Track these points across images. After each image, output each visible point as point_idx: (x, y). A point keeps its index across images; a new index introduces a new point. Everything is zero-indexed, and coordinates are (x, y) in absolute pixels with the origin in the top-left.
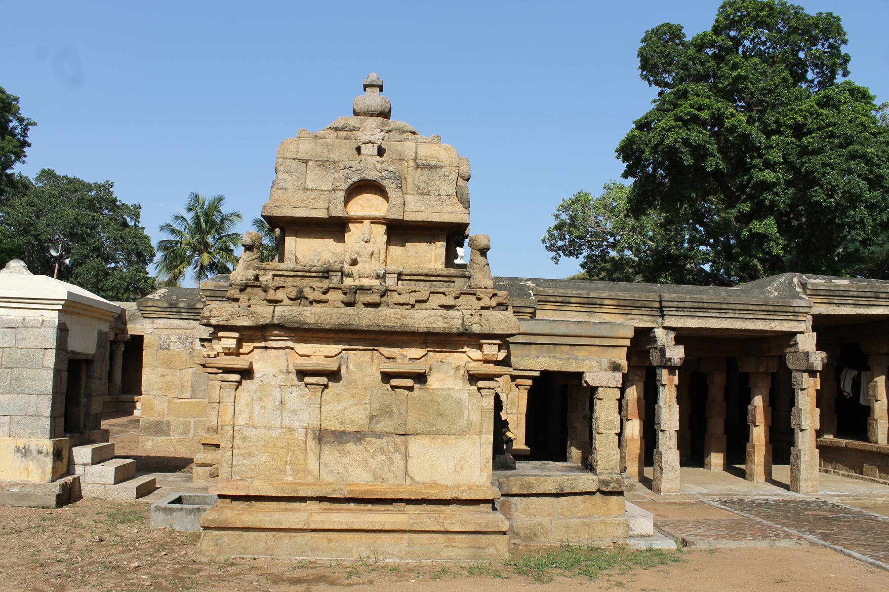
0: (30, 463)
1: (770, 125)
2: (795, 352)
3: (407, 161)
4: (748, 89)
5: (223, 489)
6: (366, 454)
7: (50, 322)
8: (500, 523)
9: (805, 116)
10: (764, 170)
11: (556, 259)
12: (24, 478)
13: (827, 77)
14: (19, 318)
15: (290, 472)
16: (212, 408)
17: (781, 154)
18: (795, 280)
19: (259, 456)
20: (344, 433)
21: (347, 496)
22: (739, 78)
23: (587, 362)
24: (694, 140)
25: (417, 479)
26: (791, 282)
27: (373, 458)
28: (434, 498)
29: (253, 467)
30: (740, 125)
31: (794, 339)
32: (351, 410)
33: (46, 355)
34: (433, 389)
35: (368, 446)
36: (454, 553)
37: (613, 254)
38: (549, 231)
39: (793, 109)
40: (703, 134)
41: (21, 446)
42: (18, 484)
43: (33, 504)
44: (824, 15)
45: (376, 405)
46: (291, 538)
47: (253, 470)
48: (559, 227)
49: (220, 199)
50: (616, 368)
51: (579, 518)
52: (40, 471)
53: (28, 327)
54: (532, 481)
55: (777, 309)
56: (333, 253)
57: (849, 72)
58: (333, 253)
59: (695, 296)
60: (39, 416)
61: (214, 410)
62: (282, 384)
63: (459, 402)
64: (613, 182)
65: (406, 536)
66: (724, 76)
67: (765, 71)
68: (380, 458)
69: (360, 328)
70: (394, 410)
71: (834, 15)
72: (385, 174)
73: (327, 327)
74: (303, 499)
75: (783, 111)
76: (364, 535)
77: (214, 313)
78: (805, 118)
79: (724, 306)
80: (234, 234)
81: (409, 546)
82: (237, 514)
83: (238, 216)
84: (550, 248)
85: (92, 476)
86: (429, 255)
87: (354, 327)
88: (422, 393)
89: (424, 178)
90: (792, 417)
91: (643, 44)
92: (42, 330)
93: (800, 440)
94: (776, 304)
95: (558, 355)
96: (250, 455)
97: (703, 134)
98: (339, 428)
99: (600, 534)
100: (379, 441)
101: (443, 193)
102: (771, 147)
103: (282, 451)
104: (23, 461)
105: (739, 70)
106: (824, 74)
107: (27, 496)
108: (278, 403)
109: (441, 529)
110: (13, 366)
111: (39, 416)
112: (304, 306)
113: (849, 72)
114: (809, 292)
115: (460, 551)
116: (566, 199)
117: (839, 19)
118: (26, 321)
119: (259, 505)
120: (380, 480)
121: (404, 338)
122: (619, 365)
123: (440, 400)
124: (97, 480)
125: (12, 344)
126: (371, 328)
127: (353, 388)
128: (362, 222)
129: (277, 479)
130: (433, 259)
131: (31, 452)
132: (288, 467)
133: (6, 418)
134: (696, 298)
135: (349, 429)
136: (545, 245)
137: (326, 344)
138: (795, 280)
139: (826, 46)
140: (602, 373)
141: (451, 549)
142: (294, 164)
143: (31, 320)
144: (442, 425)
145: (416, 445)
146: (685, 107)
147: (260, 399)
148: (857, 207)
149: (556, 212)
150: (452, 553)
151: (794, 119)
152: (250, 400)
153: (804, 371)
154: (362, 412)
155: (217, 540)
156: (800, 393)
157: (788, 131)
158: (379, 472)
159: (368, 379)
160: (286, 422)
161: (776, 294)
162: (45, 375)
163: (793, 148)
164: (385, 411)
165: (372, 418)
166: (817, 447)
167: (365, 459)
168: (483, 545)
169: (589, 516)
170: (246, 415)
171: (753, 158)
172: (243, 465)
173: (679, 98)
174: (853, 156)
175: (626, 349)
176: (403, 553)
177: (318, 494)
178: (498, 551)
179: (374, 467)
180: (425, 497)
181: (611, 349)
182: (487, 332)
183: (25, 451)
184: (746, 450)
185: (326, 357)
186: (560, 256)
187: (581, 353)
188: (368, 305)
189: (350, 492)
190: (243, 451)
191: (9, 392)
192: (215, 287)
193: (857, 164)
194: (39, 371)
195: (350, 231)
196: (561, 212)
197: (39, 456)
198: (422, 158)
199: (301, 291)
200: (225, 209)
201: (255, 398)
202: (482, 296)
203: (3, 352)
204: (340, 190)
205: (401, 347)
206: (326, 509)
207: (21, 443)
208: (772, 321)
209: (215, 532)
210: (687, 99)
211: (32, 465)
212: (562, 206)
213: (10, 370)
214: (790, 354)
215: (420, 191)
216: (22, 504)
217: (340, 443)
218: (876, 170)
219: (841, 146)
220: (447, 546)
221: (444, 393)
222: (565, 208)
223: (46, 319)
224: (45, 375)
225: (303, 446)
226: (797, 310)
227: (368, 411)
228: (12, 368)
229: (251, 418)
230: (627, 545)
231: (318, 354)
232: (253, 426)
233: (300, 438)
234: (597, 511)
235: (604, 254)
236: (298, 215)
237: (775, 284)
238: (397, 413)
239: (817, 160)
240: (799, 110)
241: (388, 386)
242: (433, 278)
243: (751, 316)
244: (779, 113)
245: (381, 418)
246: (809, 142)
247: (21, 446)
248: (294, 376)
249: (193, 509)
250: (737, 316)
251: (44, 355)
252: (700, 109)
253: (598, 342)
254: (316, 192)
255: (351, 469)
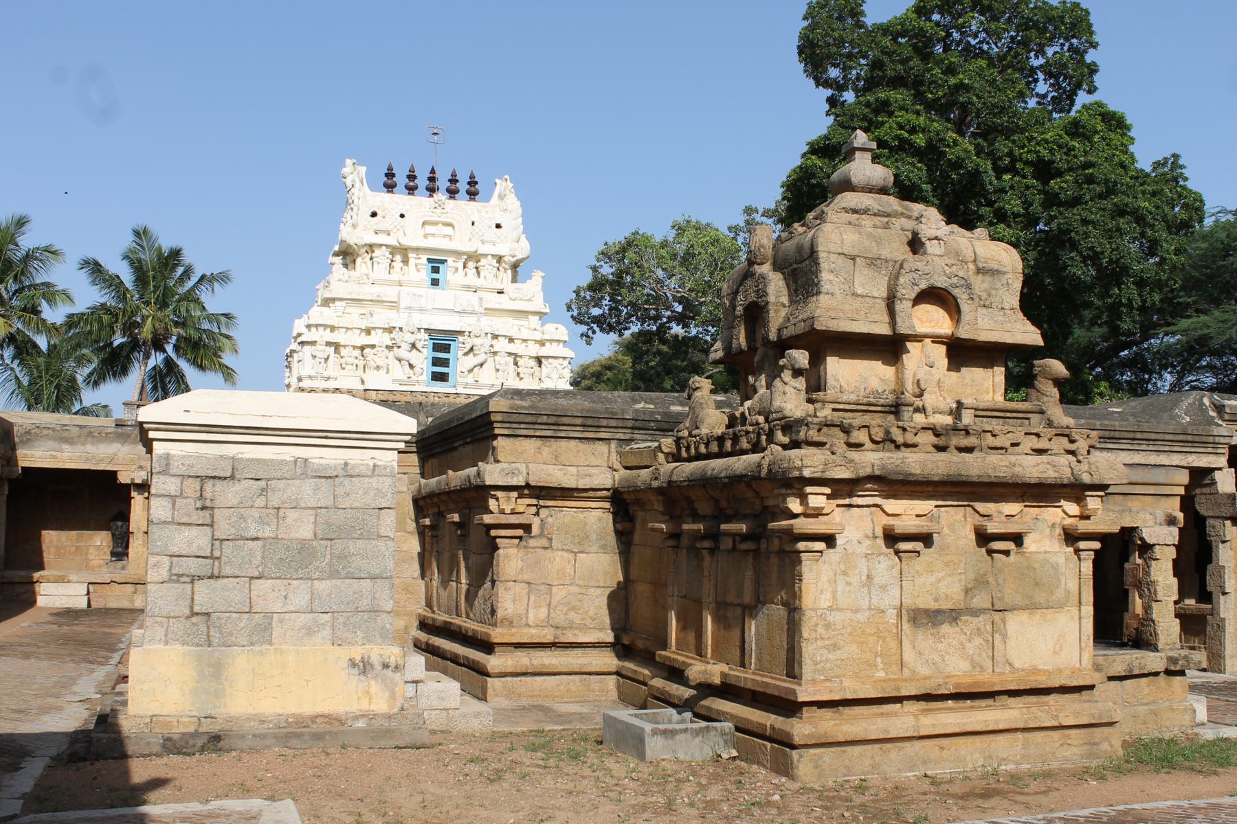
0: (373, 682)
1: (1000, 158)
2: (1210, 494)
3: (966, 263)
4: (973, 104)
5: (815, 694)
6: (962, 638)
7: (385, 468)
8: (1113, 713)
9: (1052, 149)
10: (996, 224)
11: (587, 336)
12: (364, 706)
13: (1065, 92)
14: (338, 462)
15: (881, 666)
16: (506, 589)
17: (1019, 202)
18: (1206, 401)
19: (846, 648)
20: (939, 612)
21: (954, 691)
22: (961, 87)
23: (1141, 515)
24: (906, 176)
25: (1017, 665)
26: (1202, 404)
27: (970, 642)
28: (1042, 686)
29: (839, 662)
30: (969, 158)
31: (1209, 477)
32: (945, 582)
33: (382, 517)
34: (1031, 552)
35: (963, 627)
36: (1069, 752)
37: (677, 329)
38: (577, 292)
39: (1033, 138)
40: (918, 169)
41: (358, 658)
42: (363, 716)
43: (401, 743)
44: (1069, 5)
45: (972, 576)
46: (900, 749)
47: (838, 666)
48: (597, 286)
49: (21, 223)
50: (1171, 521)
51: (1144, 704)
52: (387, 694)
53: (352, 476)
54: (1101, 662)
55: (1196, 439)
56: (881, 380)
57: (1096, 88)
58: (881, 380)
59: (1106, 422)
60: (377, 611)
61: (510, 592)
62: (868, 552)
63: (1055, 568)
64: (687, 218)
65: (1019, 735)
66: (935, 82)
67: (995, 80)
68: (978, 641)
69: (970, 480)
70: (991, 580)
71: (1082, 6)
72: (955, 280)
73: (936, 479)
74: (899, 700)
75: (1019, 139)
76: (977, 739)
77: (807, 462)
78: (1051, 151)
79: (1138, 436)
80: (43, 284)
81: (1024, 748)
82: (835, 725)
83: (54, 253)
84: (578, 320)
85: (428, 697)
86: (986, 384)
87: (964, 479)
88: (1019, 557)
89: (985, 285)
90: (1208, 578)
91: (806, 23)
92: (374, 480)
93: (1222, 606)
94: (1195, 432)
95: (1111, 507)
96: (835, 647)
97: (918, 169)
98: (933, 606)
99: (1168, 723)
100: (975, 620)
101: (1007, 306)
102: (1003, 191)
103: (871, 639)
104: (362, 681)
105: (961, 76)
106: (1060, 87)
107: (388, 733)
108: (864, 577)
109: (1056, 724)
110: (334, 536)
111: (377, 611)
112: (889, 450)
113: (1096, 88)
114: (1227, 417)
115: (1075, 750)
116: (610, 243)
117: (1087, 13)
118: (349, 467)
119: (847, 711)
120: (978, 668)
121: (1002, 490)
122: (1175, 517)
123: (1036, 566)
124: (436, 704)
125: (330, 503)
126: (981, 480)
127: (947, 555)
128: (921, 341)
129: (868, 676)
130: (991, 389)
131: (372, 666)
132: (879, 659)
133: (327, 617)
134: (1106, 425)
135: (944, 607)
136: (570, 313)
137: (918, 499)
138: (1206, 401)
139: (1066, 48)
140: (1158, 528)
141: (1065, 747)
142: (841, 261)
143: (357, 466)
144: (1040, 597)
145: (1015, 623)
146: (890, 128)
147: (845, 573)
148: (1123, 283)
149: (594, 263)
150: (1068, 752)
151: (1036, 152)
152: (832, 575)
153: (1227, 519)
154: (957, 584)
155: (816, 761)
156: (1221, 546)
157: (1026, 170)
158: (977, 658)
159: (962, 542)
160: (875, 600)
161: (1188, 419)
162: (383, 549)
163: (1034, 195)
164: (980, 582)
165: (967, 591)
166: (1176, 616)
167: (961, 643)
168: (1097, 741)
169: (1154, 702)
170: (829, 595)
171: (980, 205)
172: (828, 660)
173: (877, 112)
174: (1121, 212)
175: (1178, 498)
176: (1018, 757)
177: (922, 691)
178: (1111, 746)
179: (971, 652)
180: (1034, 685)
181: (1164, 498)
182: (1097, 482)
183: (364, 666)
184: (1122, 623)
185: (917, 516)
186: (594, 332)
187: (1134, 503)
188: (962, 450)
189: (957, 685)
190: (827, 643)
191: (331, 577)
192: (511, 408)
193: (1127, 223)
194: (373, 542)
195: (909, 352)
196: (602, 263)
197: (385, 671)
198: (982, 260)
199: (887, 432)
200: (27, 242)
201: (838, 571)
202: (1077, 437)
203: (316, 515)
204: (907, 300)
205: (996, 502)
206: (925, 710)
207: (357, 653)
208: (1188, 455)
209: (812, 751)
210: (891, 114)
211: (375, 687)
212: (603, 253)
213: (329, 542)
214: (1203, 497)
215: (982, 303)
216: (382, 743)
217: (934, 625)
218: (1149, 232)
219: (1101, 196)
220: (1062, 745)
221: (1041, 557)
222: (606, 255)
223: (379, 463)
224: (383, 549)
225: (895, 631)
226: (1217, 439)
227: (963, 583)
228: (331, 540)
229: (835, 598)
230: (1196, 734)
231: (909, 512)
232: (838, 609)
233: (891, 621)
234: (1162, 695)
235: (663, 329)
236: (857, 331)
237: (1185, 405)
238: (995, 584)
239: (1075, 214)
240: (1042, 140)
241: (984, 550)
242: (1008, 415)
243: (1167, 449)
244: (1014, 142)
245: (976, 591)
246: (1061, 188)
247: (358, 658)
248: (880, 542)
249: (700, 728)
250: (1151, 448)
251: (379, 518)
252: (913, 131)
253: (1152, 490)
254: (867, 299)
255: (947, 657)
